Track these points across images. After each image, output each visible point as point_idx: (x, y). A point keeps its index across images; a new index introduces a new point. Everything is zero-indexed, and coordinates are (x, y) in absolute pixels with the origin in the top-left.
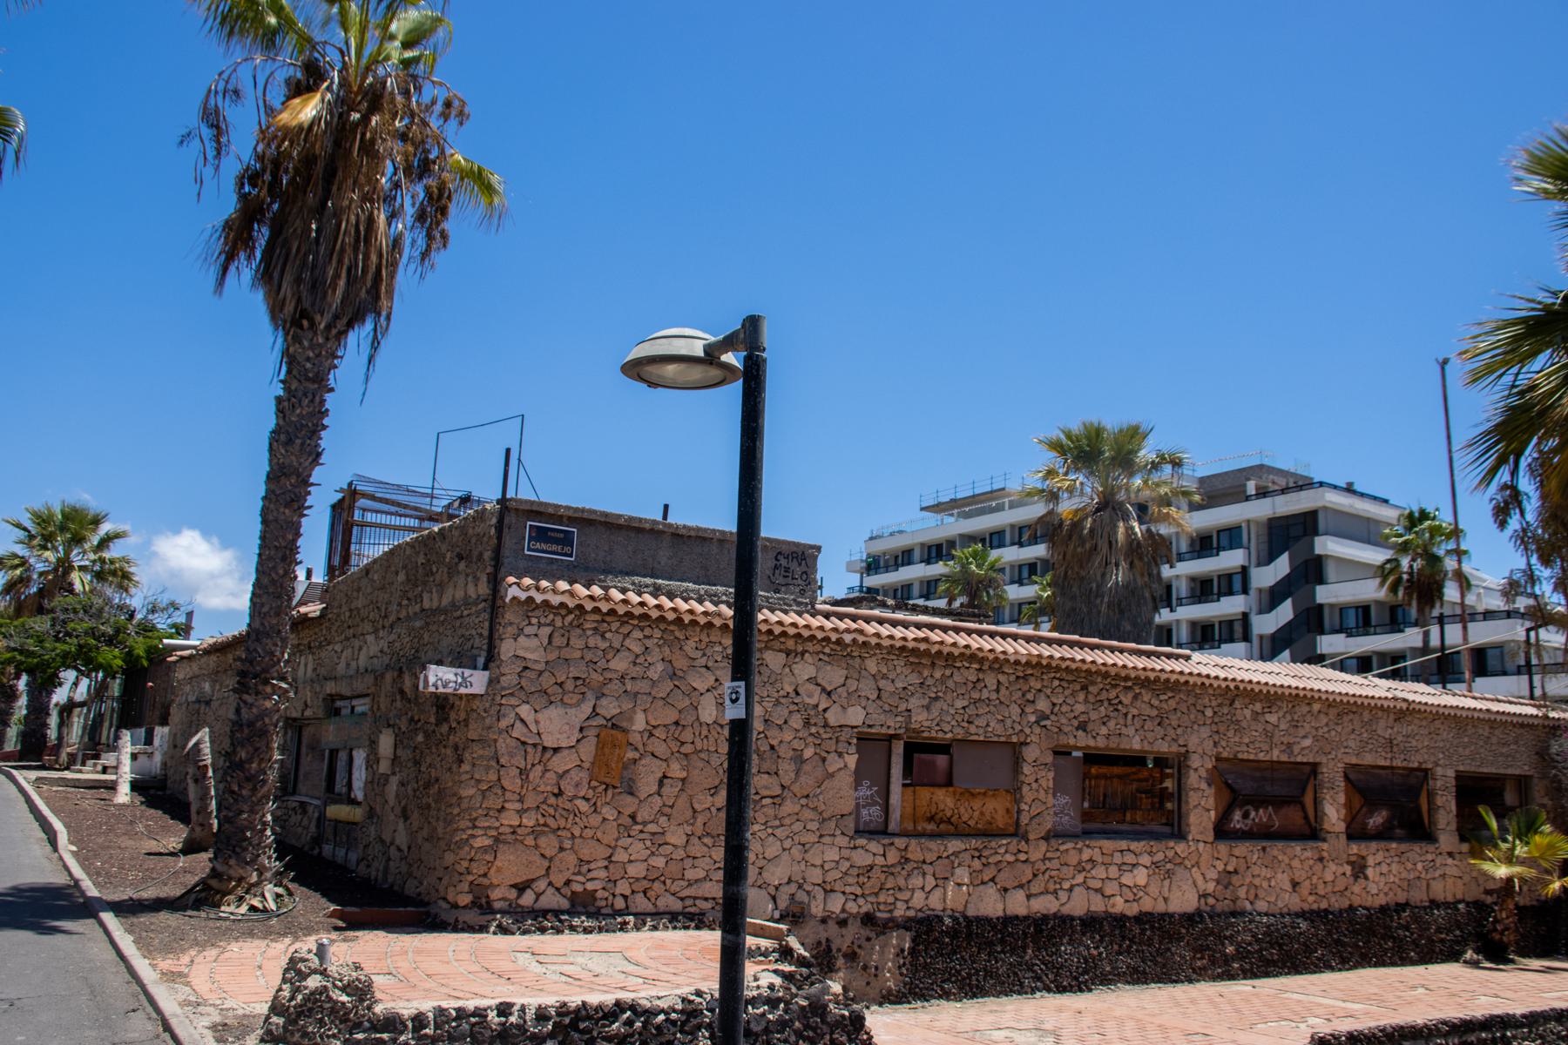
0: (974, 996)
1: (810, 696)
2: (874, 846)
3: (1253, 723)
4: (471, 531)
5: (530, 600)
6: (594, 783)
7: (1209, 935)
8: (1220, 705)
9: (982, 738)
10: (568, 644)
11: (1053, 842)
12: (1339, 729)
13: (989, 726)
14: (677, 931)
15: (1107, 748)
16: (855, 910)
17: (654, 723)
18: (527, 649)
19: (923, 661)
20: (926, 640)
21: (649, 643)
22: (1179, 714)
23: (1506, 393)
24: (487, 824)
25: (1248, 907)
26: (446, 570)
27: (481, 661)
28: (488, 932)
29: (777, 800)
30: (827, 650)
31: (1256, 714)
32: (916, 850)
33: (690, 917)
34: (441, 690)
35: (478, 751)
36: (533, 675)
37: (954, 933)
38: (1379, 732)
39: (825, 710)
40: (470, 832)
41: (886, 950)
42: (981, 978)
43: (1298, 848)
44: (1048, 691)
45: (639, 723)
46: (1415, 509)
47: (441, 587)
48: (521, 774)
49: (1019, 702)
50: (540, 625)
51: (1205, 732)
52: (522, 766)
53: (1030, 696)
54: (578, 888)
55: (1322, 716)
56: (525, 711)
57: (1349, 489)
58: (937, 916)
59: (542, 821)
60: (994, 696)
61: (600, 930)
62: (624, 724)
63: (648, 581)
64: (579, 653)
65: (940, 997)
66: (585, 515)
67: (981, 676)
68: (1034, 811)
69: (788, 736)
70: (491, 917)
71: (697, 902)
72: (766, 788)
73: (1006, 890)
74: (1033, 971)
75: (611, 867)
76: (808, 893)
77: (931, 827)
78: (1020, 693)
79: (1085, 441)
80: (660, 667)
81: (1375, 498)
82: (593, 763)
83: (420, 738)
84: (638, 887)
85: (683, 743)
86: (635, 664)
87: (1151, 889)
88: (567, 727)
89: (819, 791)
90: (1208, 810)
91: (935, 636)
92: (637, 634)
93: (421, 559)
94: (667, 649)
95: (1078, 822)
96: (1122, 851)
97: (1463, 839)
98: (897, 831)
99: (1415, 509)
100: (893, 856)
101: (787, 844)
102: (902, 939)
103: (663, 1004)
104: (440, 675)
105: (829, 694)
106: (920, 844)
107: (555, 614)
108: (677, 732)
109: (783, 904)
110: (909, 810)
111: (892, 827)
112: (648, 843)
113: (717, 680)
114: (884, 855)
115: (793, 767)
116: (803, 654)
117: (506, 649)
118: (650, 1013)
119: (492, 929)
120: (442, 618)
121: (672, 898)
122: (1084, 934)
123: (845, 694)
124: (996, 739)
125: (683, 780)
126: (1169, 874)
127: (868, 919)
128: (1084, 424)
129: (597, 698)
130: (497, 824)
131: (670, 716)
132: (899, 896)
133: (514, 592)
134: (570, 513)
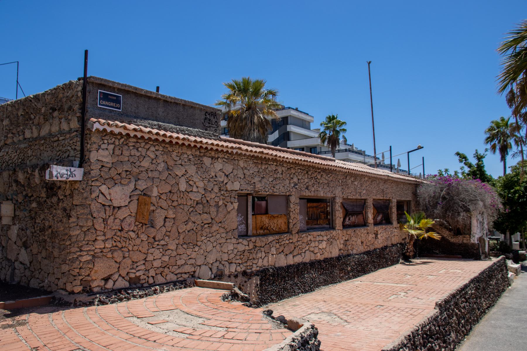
0: (281, 299)
1: (221, 177)
2: (245, 242)
4: (61, 95)
5: (105, 130)
6: (137, 223)
7: (344, 264)
9: (278, 194)
10: (122, 154)
11: (300, 234)
13: (280, 189)
14: (177, 290)
15: (314, 196)
16: (239, 271)
17: (161, 192)
18: (103, 156)
20: (262, 153)
21: (158, 153)
23: (510, 55)
24: (88, 249)
25: (351, 252)
26: (42, 117)
27: (77, 163)
28: (94, 305)
29: (210, 225)
30: (226, 157)
31: (352, 181)
32: (260, 241)
33: (181, 282)
34: (60, 179)
35: (80, 210)
36: (106, 170)
37: (273, 275)
38: (380, 187)
39: (226, 184)
40: (79, 253)
41: (252, 285)
44: (297, 174)
45: (155, 193)
46: (331, 115)
47: (39, 126)
48: (104, 221)
49: (289, 178)
50: (109, 144)
51: (340, 189)
52: (104, 217)
53: (292, 176)
54: (132, 276)
56: (103, 188)
57: (297, 110)
58: (267, 269)
59: (114, 245)
60: (281, 176)
61: (146, 295)
62: (149, 193)
63: (156, 123)
64: (127, 158)
65: (271, 302)
66: (127, 89)
67: (277, 168)
69: (213, 196)
70: (93, 297)
71: (183, 275)
72: (206, 220)
73: (287, 255)
74: (298, 286)
75: (146, 263)
76: (223, 265)
77: (262, 232)
78: (289, 175)
79: (242, 84)
80: (163, 165)
81: (305, 113)
82: (136, 213)
83: (34, 205)
84: (158, 271)
85: (173, 201)
86: (152, 163)
87: (327, 249)
88: (124, 196)
89: (225, 219)
90: (341, 218)
91: (266, 151)
92: (153, 149)
93: (21, 112)
94: (165, 156)
97: (398, 223)
98: (251, 235)
99: (331, 115)
100: (251, 246)
101: (215, 244)
102: (256, 280)
104: (59, 170)
105: (227, 176)
106: (260, 239)
107: (116, 138)
108: (171, 196)
109: (214, 271)
110: (254, 225)
111: (250, 233)
112: (161, 250)
113: (186, 171)
114: (248, 245)
115: (215, 210)
116: (218, 158)
117: (93, 156)
119: (96, 303)
120: (42, 142)
121: (173, 275)
122: (311, 269)
123: (233, 177)
124: (282, 194)
125: (174, 218)
127: (244, 273)
128: (243, 79)
129: (136, 181)
130: (94, 248)
131: (167, 188)
133: (96, 126)
134: (120, 87)
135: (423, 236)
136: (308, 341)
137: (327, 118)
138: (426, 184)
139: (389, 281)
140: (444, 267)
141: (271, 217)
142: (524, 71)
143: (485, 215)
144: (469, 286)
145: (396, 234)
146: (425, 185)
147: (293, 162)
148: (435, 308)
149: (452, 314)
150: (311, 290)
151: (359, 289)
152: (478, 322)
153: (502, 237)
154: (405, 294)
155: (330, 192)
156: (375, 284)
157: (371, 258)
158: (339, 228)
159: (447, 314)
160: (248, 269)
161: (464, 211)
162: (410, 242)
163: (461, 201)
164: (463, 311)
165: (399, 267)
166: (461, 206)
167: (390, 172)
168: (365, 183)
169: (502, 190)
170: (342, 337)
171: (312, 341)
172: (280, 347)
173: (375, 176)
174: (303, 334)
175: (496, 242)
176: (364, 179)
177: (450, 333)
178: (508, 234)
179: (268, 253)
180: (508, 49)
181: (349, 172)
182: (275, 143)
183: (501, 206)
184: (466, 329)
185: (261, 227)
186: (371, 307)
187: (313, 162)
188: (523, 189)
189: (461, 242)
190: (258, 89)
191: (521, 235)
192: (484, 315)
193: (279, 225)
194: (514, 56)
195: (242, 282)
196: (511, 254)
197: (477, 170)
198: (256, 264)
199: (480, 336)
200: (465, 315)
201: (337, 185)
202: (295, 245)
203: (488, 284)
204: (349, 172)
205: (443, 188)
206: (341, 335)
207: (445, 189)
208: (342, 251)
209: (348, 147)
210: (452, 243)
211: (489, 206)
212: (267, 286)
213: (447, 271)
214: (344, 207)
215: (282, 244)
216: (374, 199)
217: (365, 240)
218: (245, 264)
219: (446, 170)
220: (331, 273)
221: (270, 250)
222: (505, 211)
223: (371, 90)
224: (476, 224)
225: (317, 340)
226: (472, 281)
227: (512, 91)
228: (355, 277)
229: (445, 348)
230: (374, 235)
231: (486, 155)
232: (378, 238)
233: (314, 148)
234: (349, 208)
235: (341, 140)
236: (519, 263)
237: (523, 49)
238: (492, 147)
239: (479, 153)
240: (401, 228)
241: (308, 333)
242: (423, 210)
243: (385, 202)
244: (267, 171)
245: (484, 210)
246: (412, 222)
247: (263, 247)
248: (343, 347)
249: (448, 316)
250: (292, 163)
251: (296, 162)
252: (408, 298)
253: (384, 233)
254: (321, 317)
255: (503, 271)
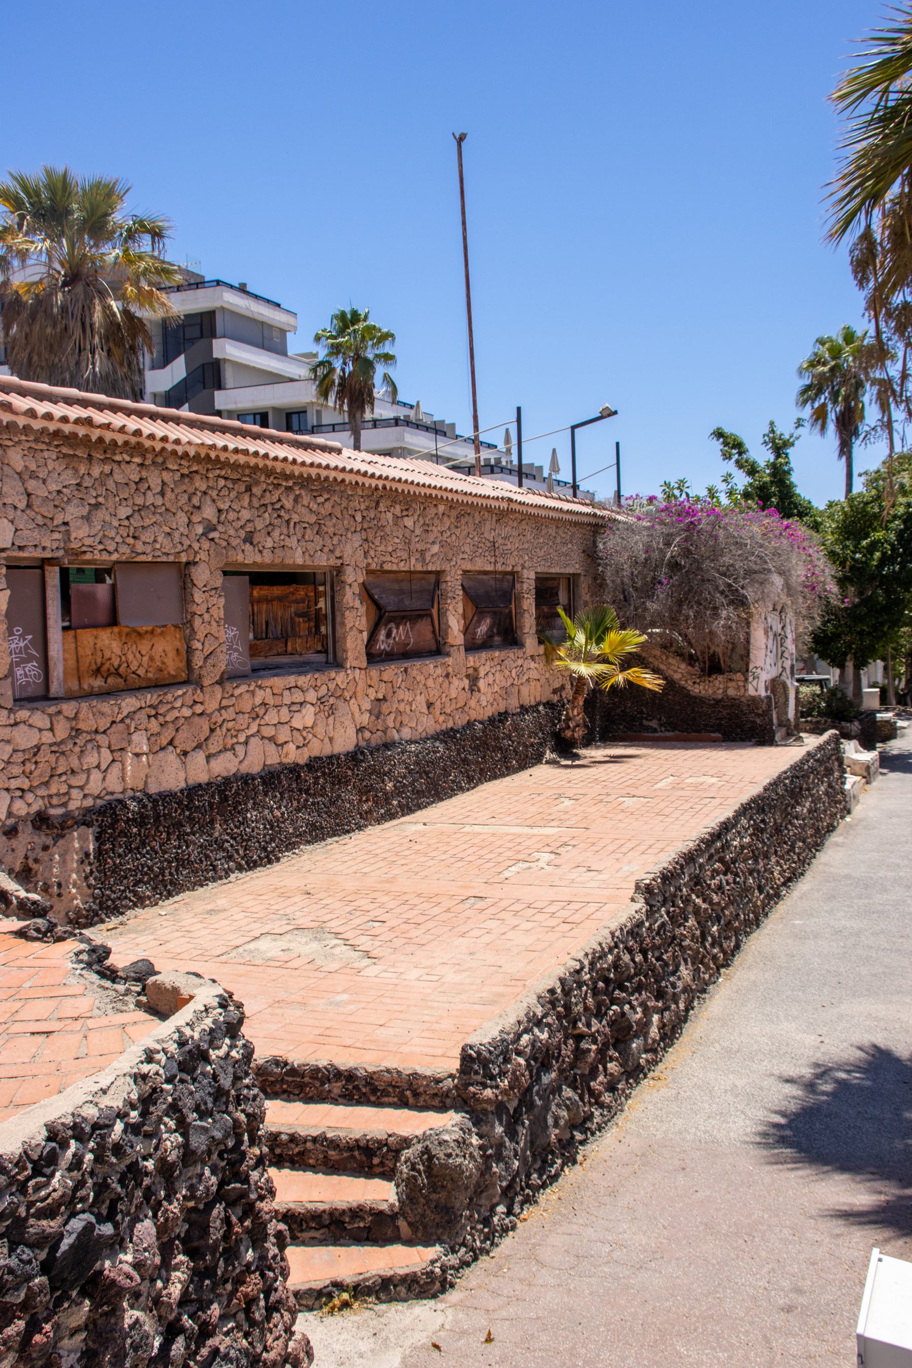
0: (170, 895)
2: (40, 719)
3: (395, 528)
7: (372, 774)
8: (367, 509)
9: (150, 559)
11: (228, 686)
12: (458, 532)
15: (272, 565)
16: (23, 813)
19: (79, 453)
20: (89, 422)
22: (334, 520)
23: (869, 118)
25: (396, 737)
31: (396, 518)
37: (141, 820)
41: (68, 857)
42: (173, 870)
43: (432, 666)
44: (214, 494)
46: (348, 310)
49: (186, 508)
51: (357, 540)
53: (196, 501)
55: (446, 518)
57: (242, 289)
58: (120, 801)
60: (159, 501)
65: (135, 905)
67: (144, 474)
68: (208, 649)
73: (185, 753)
77: (98, 683)
78: (186, 496)
81: (268, 301)
87: (320, 730)
90: (361, 632)
91: (100, 418)
95: (246, 659)
96: (290, 689)
97: (540, 642)
99: (348, 310)
102: (83, 839)
103: (115, 1101)
106: (91, 707)
110: (72, 663)
111: (55, 688)
114: (51, 729)
118: (101, 1127)
122: (266, 795)
126: (333, 709)
127: (41, 821)
132: (75, 781)
135: (612, 681)
136: (207, 1051)
137: (335, 317)
138: (625, 523)
139: (508, 819)
140: (671, 771)
141: (127, 634)
142: (905, 172)
143: (790, 616)
144: (734, 826)
145: (534, 674)
146: (620, 526)
147: (198, 455)
148: (633, 900)
149: (683, 911)
150: (269, 859)
151: (417, 847)
152: (758, 926)
153: (833, 676)
154: (553, 856)
155: (326, 550)
156: (467, 829)
157: (458, 750)
158: (355, 664)
159: (668, 913)
160: (52, 806)
161: (731, 602)
162: (575, 698)
163: (724, 575)
164: (716, 898)
165: (541, 773)
166: (722, 588)
167: (515, 488)
168: (436, 522)
169: (836, 540)
170: (352, 1008)
171: (219, 1048)
172: (96, 1088)
173: (470, 500)
174: (188, 1032)
175: (817, 689)
176: (433, 511)
177: (677, 969)
178: (850, 665)
179: (122, 749)
180: (864, 95)
181: (384, 487)
182: (173, 398)
183: (833, 588)
184: (723, 951)
185: (94, 667)
186: (448, 903)
187: (266, 456)
188: (892, 536)
189: (719, 694)
190: (99, 213)
191: (885, 668)
192: (776, 903)
193: (157, 658)
194: (880, 119)
195: (33, 849)
196: (856, 723)
197: (772, 482)
198: (81, 788)
199: (761, 965)
200: (723, 909)
201: (347, 529)
202: (213, 720)
203: (788, 815)
204: (384, 487)
205: (672, 535)
206: (349, 1002)
207: (678, 539)
208: (367, 734)
209: (402, 412)
210: (695, 698)
211: (800, 589)
212: (120, 856)
213: (678, 780)
214: (371, 597)
215: (168, 718)
216: (465, 572)
217: (440, 697)
218: (42, 792)
219: (681, 484)
220: (332, 803)
221: (130, 742)
222: (843, 602)
223: (465, 230)
224: (764, 641)
225: (240, 1043)
226: (744, 810)
227: (867, 236)
228: (407, 809)
229: (661, 1011)
230: (466, 682)
231: (797, 438)
232: (479, 691)
233: (299, 413)
234: (389, 601)
235: (380, 391)
236: (874, 748)
237: (906, 96)
238: (814, 413)
239: (778, 433)
240: (549, 657)
241: (208, 1023)
242: (614, 602)
243: (502, 580)
244: (111, 485)
245: (785, 599)
246: (581, 638)
247: (104, 732)
248: (348, 1042)
249: (671, 918)
250: (197, 458)
251: (208, 455)
252: (559, 871)
253: (497, 675)
254: (292, 945)
255: (832, 774)
